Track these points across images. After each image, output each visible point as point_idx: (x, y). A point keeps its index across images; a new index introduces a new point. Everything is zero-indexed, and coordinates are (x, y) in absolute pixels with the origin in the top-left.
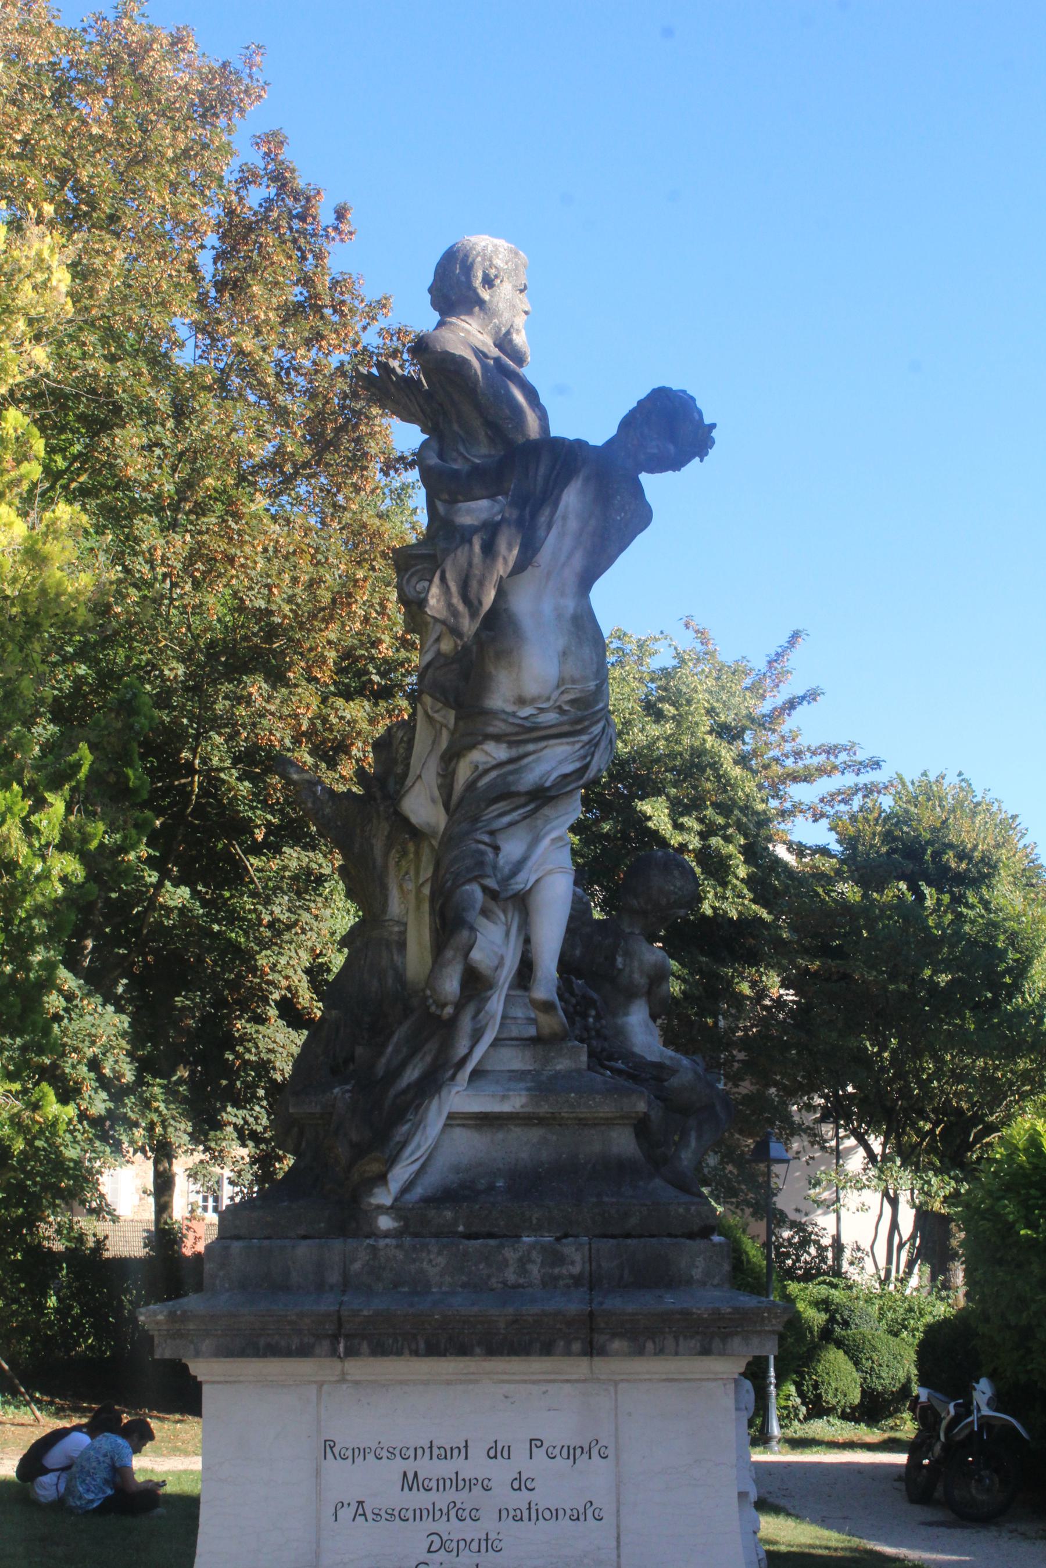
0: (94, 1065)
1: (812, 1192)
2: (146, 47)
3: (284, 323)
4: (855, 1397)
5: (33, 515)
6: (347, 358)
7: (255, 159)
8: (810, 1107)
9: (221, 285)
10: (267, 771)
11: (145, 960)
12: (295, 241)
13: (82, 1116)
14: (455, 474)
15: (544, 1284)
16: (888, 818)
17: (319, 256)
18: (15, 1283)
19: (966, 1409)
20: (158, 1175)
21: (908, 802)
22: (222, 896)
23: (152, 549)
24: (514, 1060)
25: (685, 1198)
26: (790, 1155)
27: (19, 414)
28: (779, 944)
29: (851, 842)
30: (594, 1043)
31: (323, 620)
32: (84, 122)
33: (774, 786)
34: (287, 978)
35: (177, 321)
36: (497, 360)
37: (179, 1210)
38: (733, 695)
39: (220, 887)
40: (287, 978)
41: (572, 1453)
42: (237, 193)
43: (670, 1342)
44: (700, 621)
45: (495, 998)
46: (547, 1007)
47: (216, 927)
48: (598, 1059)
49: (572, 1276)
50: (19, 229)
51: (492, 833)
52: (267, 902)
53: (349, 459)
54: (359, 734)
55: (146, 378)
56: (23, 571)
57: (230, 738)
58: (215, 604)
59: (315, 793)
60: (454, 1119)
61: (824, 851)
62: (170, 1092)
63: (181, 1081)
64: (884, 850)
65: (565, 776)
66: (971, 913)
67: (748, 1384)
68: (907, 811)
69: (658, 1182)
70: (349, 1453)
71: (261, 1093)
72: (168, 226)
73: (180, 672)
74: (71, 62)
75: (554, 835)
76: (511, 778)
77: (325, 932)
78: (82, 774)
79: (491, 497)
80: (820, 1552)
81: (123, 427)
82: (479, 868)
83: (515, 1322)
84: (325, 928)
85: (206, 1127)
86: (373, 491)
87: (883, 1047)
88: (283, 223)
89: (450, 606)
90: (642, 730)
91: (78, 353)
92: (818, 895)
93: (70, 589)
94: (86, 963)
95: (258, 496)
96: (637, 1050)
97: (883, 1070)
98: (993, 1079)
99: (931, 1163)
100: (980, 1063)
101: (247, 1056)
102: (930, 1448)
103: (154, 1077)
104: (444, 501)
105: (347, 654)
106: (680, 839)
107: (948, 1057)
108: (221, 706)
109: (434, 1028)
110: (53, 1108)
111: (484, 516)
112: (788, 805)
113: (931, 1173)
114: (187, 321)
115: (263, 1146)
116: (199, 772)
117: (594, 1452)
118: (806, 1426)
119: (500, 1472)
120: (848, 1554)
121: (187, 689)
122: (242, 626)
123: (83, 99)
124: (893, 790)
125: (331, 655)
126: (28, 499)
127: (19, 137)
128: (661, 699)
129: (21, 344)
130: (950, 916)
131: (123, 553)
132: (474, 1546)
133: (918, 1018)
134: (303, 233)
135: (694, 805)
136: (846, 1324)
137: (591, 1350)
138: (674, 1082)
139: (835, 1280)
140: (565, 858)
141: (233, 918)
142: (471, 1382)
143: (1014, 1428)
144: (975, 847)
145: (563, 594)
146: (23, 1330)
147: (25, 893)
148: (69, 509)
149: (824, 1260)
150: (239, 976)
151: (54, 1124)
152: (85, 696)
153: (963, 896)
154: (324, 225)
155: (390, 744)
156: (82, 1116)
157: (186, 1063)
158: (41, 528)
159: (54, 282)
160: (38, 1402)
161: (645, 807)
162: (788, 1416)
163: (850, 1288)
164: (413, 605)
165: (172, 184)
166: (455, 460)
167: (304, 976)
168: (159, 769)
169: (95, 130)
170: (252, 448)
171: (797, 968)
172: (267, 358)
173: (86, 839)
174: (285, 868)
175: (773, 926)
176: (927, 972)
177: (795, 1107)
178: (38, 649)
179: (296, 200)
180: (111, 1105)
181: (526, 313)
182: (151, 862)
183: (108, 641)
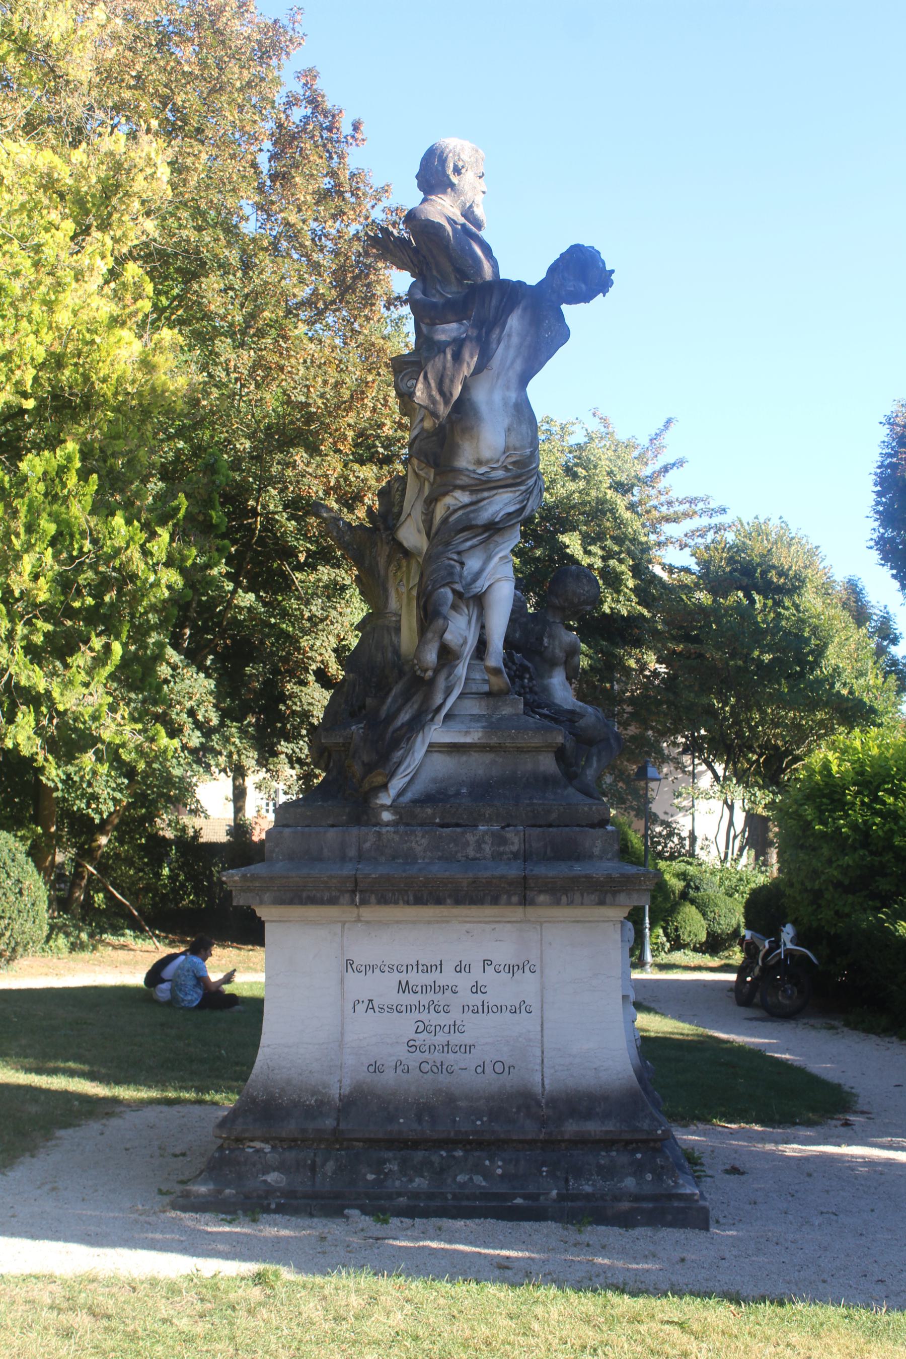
0: (192, 713)
1: (676, 801)
2: (221, 10)
3: (317, 203)
4: (703, 937)
5: (146, 336)
6: (361, 228)
7: (297, 88)
8: (675, 744)
9: (274, 177)
10: (307, 514)
11: (225, 643)
12: (324, 146)
13: (184, 747)
14: (434, 306)
15: (493, 858)
16: (731, 548)
17: (341, 157)
18: (141, 858)
19: (776, 945)
20: (235, 787)
21: (745, 537)
22: (276, 599)
23: (228, 361)
24: (474, 707)
25: (590, 801)
26: (661, 776)
27: (135, 266)
28: (655, 633)
29: (705, 564)
30: (528, 696)
31: (345, 410)
32: (179, 63)
33: (653, 525)
34: (321, 655)
35: (243, 202)
36: (463, 225)
37: (249, 813)
38: (626, 462)
39: (275, 593)
40: (321, 655)
41: (511, 969)
42: (284, 112)
43: (577, 897)
44: (602, 412)
45: (461, 665)
46: (496, 672)
47: (273, 620)
48: (531, 707)
49: (512, 853)
50: (135, 138)
51: (459, 553)
52: (307, 603)
53: (363, 299)
54: (369, 488)
55: (223, 242)
56: (139, 375)
57: (281, 491)
58: (271, 398)
59: (338, 526)
60: (433, 748)
61: (687, 570)
62: (243, 731)
63: (249, 725)
64: (728, 569)
65: (509, 514)
66: (787, 613)
67: (630, 925)
68: (744, 543)
69: (571, 790)
70: (363, 968)
71: (304, 732)
72: (237, 136)
73: (247, 446)
74: (169, 20)
75: (501, 555)
76: (472, 515)
77: (346, 624)
78: (182, 512)
79: (459, 321)
80: (677, 1037)
81: (207, 277)
82: (449, 578)
83: (474, 882)
84: (346, 621)
85: (267, 755)
86: (379, 321)
87: (726, 703)
88: (317, 133)
89: (430, 396)
90: (563, 486)
91: (176, 225)
92: (682, 600)
93: (172, 388)
94: (186, 645)
95: (300, 324)
96: (557, 701)
97: (725, 719)
98: (800, 726)
99: (756, 782)
100: (791, 714)
101: (294, 708)
102: (752, 970)
103: (232, 721)
104: (427, 324)
105: (361, 434)
106: (588, 561)
107: (769, 711)
108: (275, 469)
109: (420, 685)
110: (164, 740)
111: (454, 334)
112: (662, 538)
113: (756, 789)
114: (250, 202)
115: (305, 768)
116: (261, 515)
117: (527, 968)
118: (669, 956)
119: (464, 982)
120: (696, 1038)
121: (252, 458)
122: (290, 415)
123: (178, 46)
124: (734, 529)
125: (350, 434)
126: (142, 326)
127: (134, 73)
128: (576, 465)
129: (137, 219)
130: (772, 615)
131: (207, 363)
132: (446, 1029)
133: (748, 683)
134: (330, 140)
135: (599, 538)
136: (697, 889)
137: (525, 902)
138: (582, 723)
139: (690, 860)
140: (509, 571)
141: (285, 614)
142: (443, 922)
143: (808, 956)
144: (790, 568)
145: (508, 388)
146: (147, 889)
147: (143, 596)
148: (170, 332)
149: (683, 846)
150: (289, 653)
151: (165, 751)
152: (183, 463)
153: (782, 601)
154: (344, 134)
155: (390, 492)
156: (184, 747)
157: (254, 713)
158: (151, 345)
159: (158, 175)
160: (157, 937)
161: (565, 539)
162: (655, 951)
163: (700, 865)
164: (405, 397)
165: (239, 106)
166: (434, 296)
167: (333, 655)
168: (233, 513)
169: (187, 68)
170: (296, 291)
171: (668, 650)
172: (305, 228)
173: (184, 559)
174: (319, 580)
175: (652, 620)
176: (756, 653)
177: (665, 744)
178: (150, 429)
179: (326, 117)
180: (203, 740)
181: (484, 192)
182: (228, 576)
183: (198, 425)
